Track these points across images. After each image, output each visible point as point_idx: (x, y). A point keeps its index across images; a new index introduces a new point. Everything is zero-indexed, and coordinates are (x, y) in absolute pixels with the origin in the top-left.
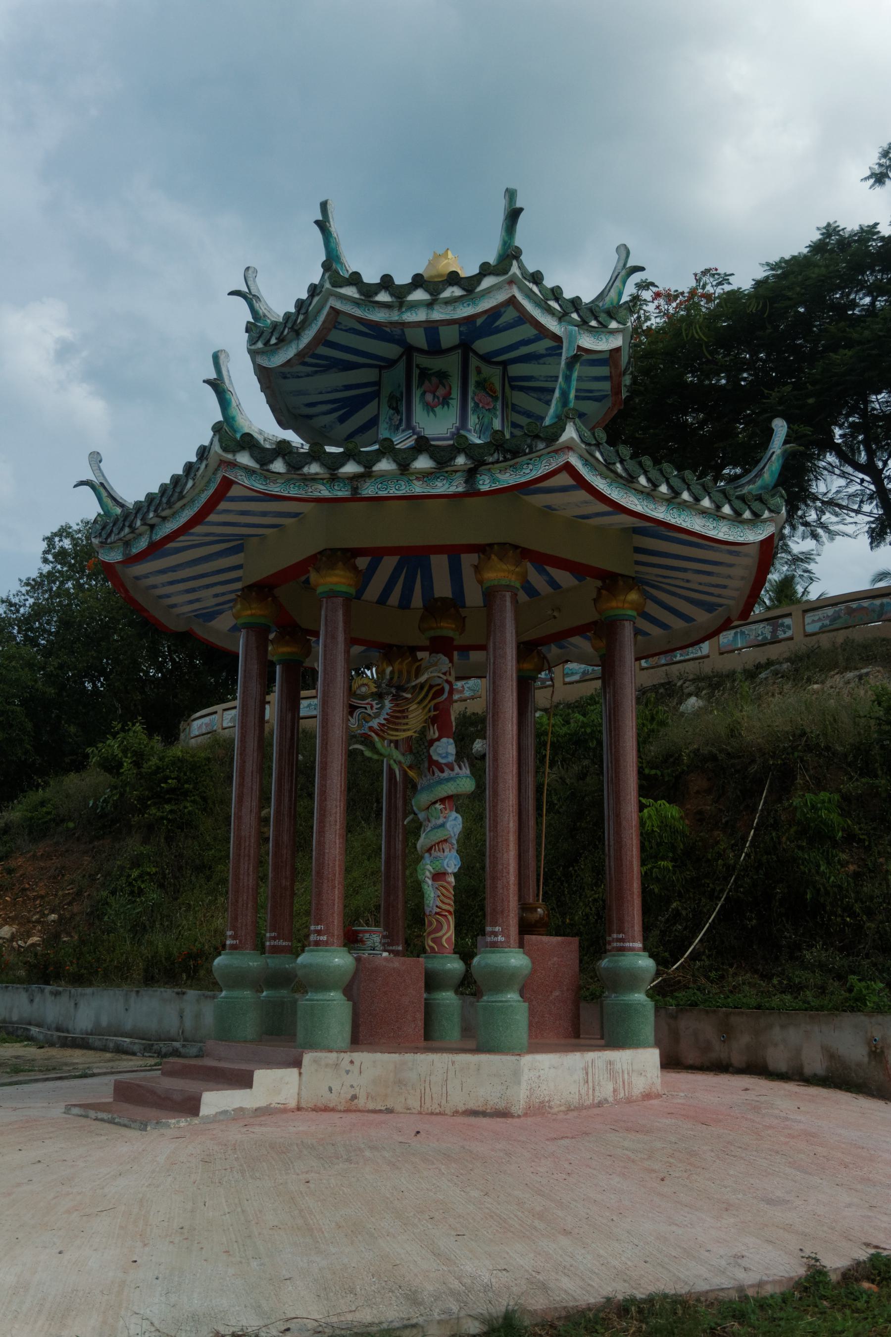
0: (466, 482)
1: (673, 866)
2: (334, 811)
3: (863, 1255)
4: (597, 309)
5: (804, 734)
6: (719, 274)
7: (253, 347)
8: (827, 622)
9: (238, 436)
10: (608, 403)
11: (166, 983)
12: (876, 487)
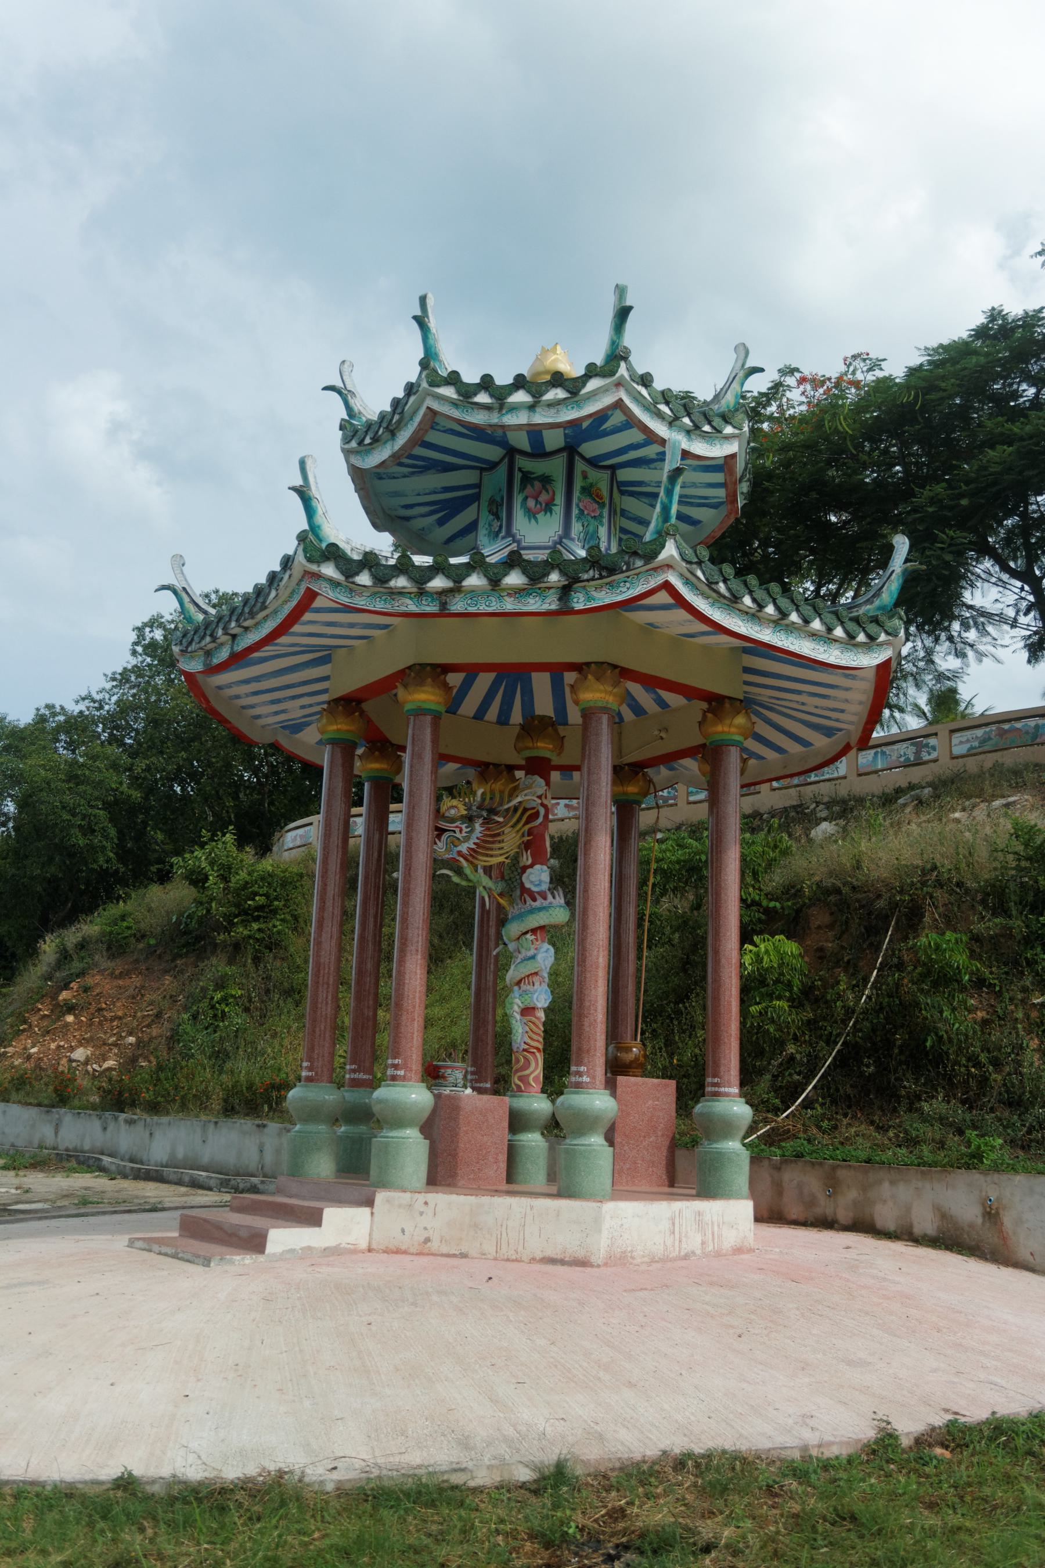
0: (560, 599)
1: (789, 1007)
2: (416, 940)
3: (939, 1420)
4: (711, 413)
5: (935, 868)
6: (871, 359)
7: (346, 446)
8: (976, 744)
9: (324, 545)
10: (724, 510)
11: (247, 1115)
12: (1035, 597)
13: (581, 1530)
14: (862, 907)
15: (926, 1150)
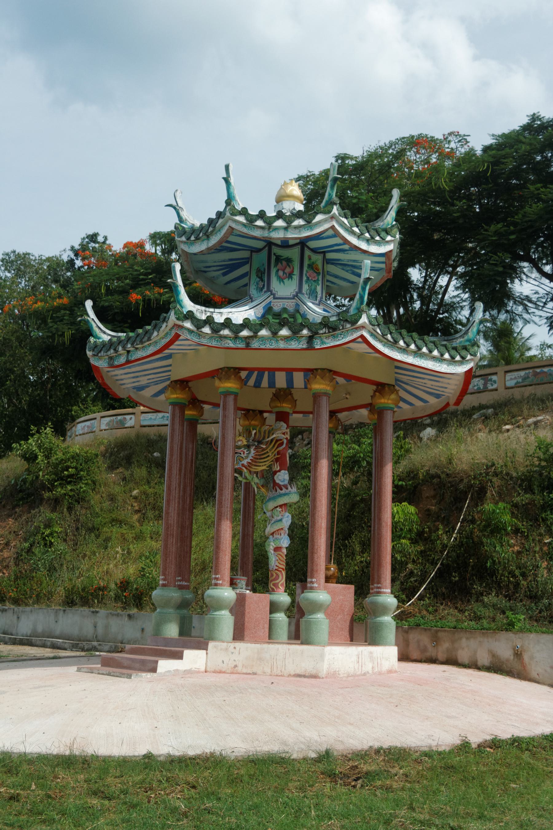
0: (308, 343)
3: (489, 738)
5: (493, 465)
8: (520, 380)
13: (341, 773)
14: (452, 486)
15: (485, 622)
